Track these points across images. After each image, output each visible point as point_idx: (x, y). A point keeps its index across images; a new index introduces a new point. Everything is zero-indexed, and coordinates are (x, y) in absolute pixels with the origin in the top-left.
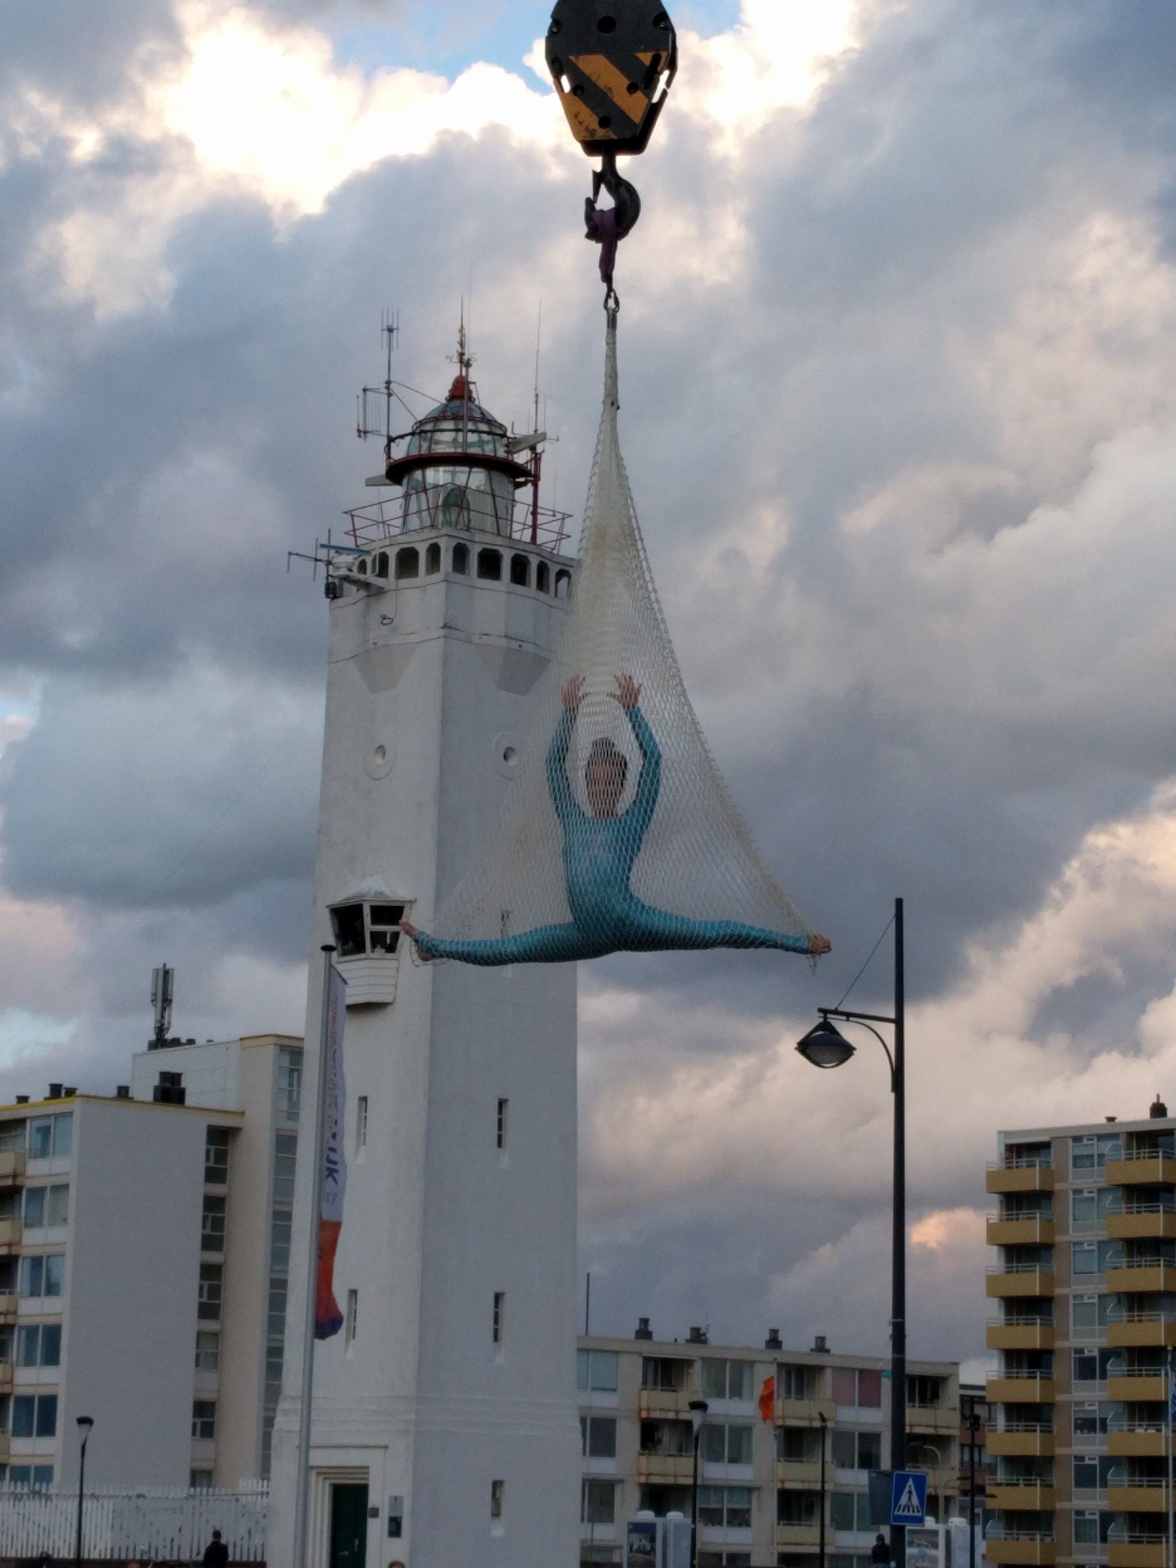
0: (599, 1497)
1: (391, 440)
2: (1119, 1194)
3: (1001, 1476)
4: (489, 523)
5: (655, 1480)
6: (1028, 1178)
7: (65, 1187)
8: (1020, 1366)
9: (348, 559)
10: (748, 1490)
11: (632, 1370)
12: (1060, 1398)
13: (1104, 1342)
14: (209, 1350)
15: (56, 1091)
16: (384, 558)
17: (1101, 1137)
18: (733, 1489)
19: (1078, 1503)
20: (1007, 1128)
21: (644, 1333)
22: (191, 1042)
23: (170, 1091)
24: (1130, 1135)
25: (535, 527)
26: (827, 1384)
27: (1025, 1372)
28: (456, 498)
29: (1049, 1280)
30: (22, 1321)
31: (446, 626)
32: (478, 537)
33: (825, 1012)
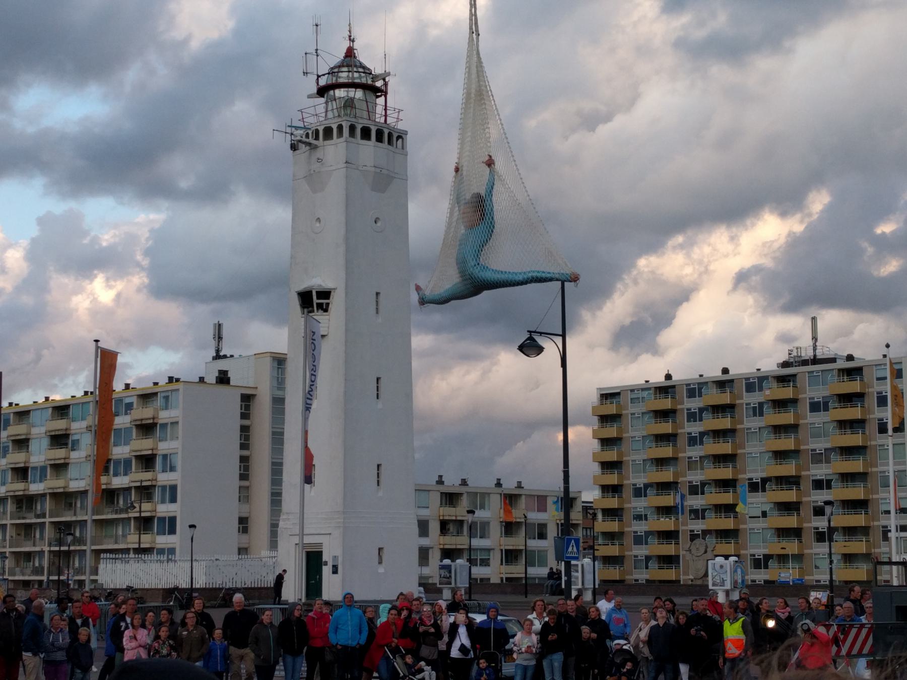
0: (424, 555)
1: (319, 76)
2: (651, 415)
3: (600, 541)
4: (365, 114)
5: (446, 547)
6: (611, 407)
7: (177, 423)
8: (608, 492)
9: (300, 132)
10: (489, 550)
11: (436, 498)
12: (626, 506)
13: (646, 481)
14: (245, 495)
15: (171, 379)
16: (317, 131)
17: (643, 390)
18: (481, 550)
19: (635, 552)
20: (602, 387)
21: (440, 482)
22: (232, 356)
23: (223, 379)
24: (656, 388)
25: (386, 116)
26: (523, 502)
27: (849, 431)
28: (349, 103)
29: (620, 454)
30: (159, 484)
31: (346, 162)
32: (361, 121)
33: (530, 332)
